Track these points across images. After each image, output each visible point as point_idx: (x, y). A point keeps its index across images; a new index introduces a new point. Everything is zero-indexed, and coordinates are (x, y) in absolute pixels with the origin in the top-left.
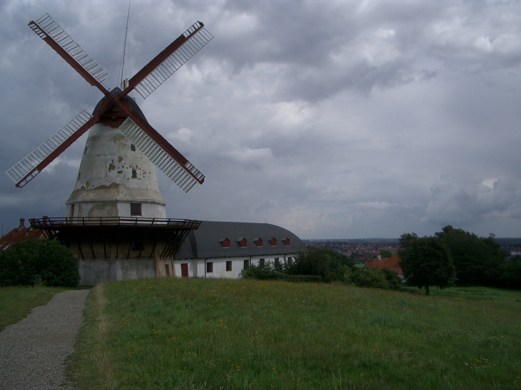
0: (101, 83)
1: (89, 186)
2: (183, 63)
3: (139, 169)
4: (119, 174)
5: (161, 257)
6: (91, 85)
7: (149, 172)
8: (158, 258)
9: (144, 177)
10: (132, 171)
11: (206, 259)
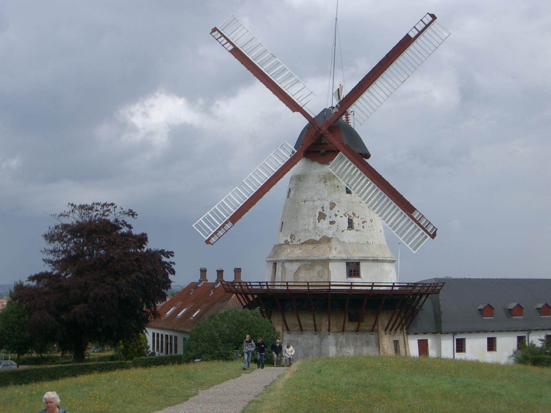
0: (303, 108)
1: (294, 240)
2: (409, 73)
3: (357, 217)
4: (331, 225)
5: (386, 330)
6: (292, 112)
7: (370, 220)
9: (363, 227)
10: (347, 220)
11: (454, 333)
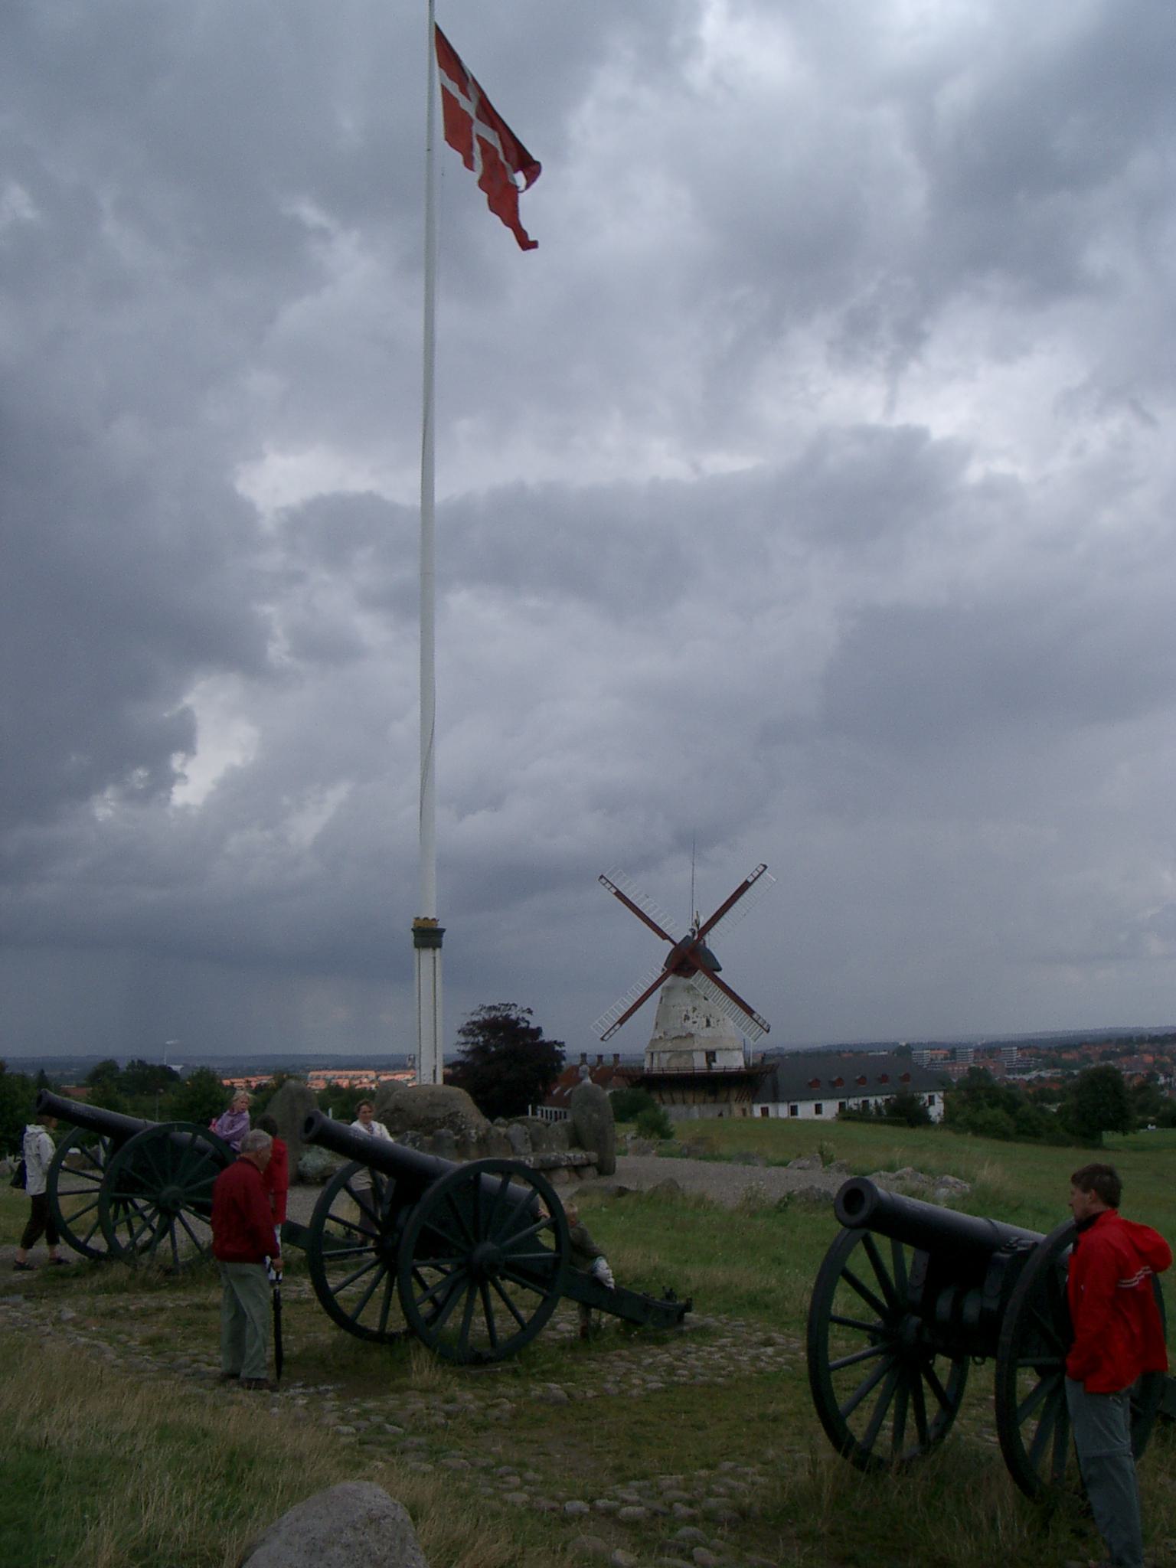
5: (736, 1100)
8: (733, 1103)
11: (789, 1102)
